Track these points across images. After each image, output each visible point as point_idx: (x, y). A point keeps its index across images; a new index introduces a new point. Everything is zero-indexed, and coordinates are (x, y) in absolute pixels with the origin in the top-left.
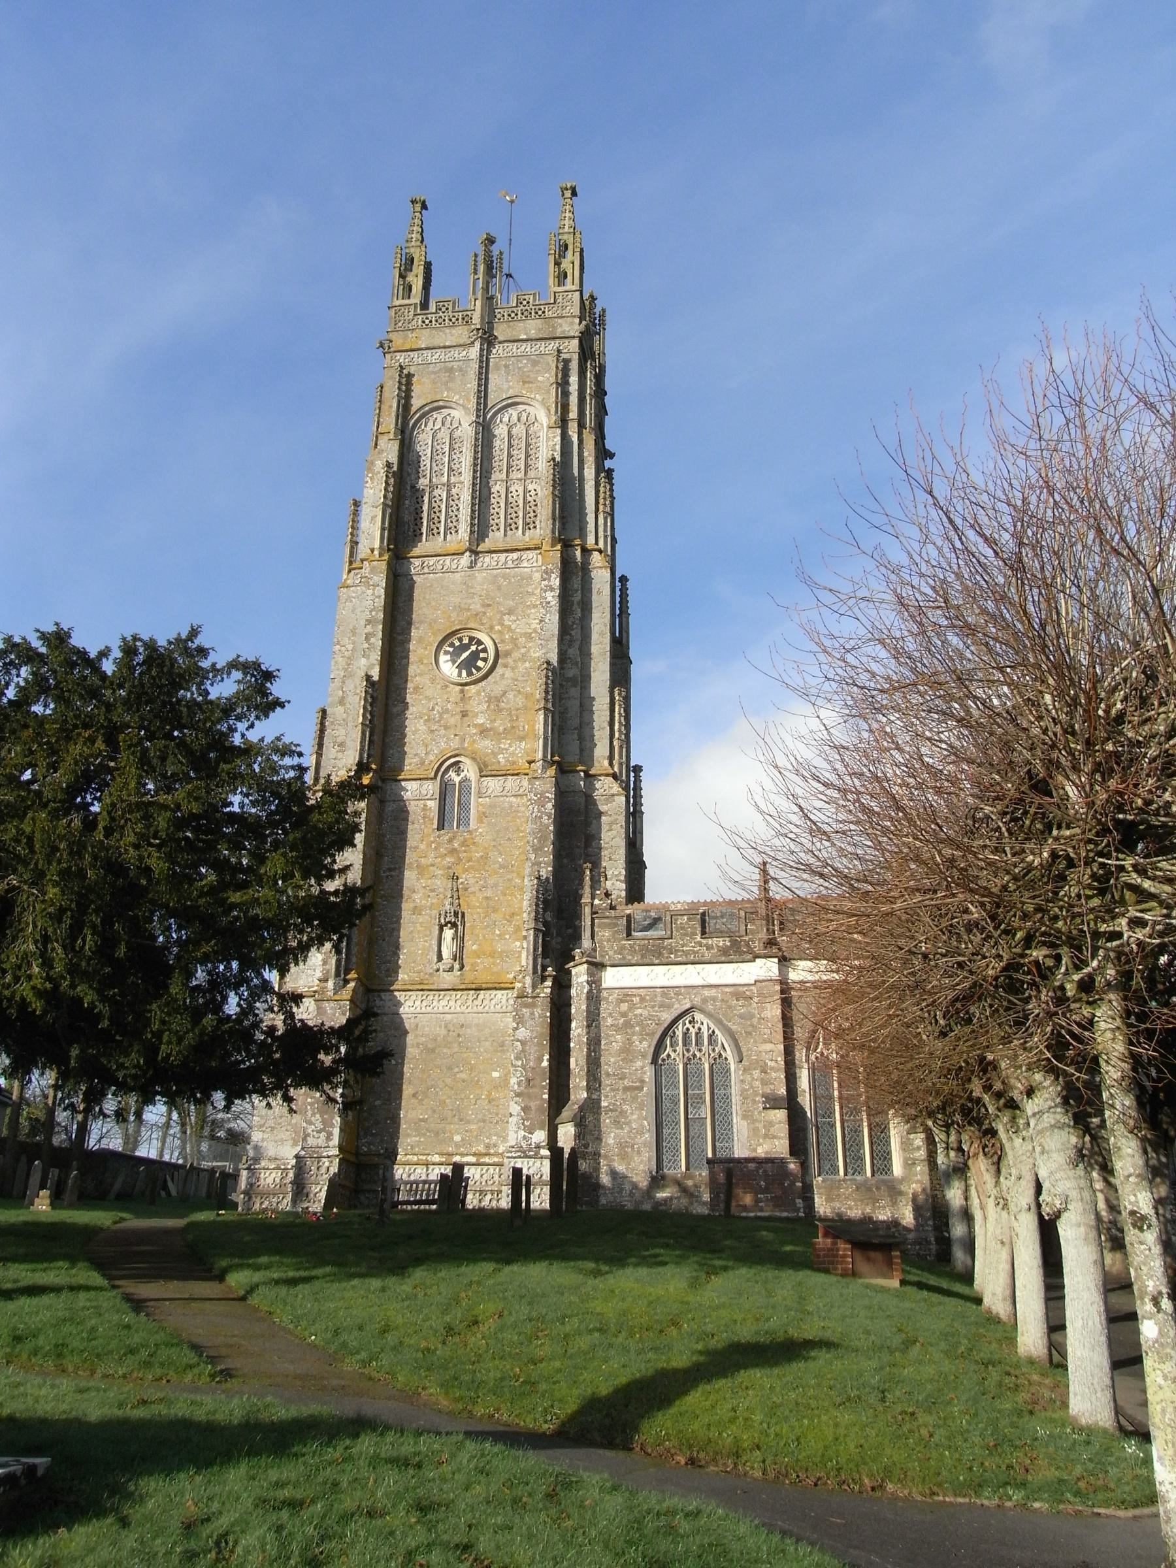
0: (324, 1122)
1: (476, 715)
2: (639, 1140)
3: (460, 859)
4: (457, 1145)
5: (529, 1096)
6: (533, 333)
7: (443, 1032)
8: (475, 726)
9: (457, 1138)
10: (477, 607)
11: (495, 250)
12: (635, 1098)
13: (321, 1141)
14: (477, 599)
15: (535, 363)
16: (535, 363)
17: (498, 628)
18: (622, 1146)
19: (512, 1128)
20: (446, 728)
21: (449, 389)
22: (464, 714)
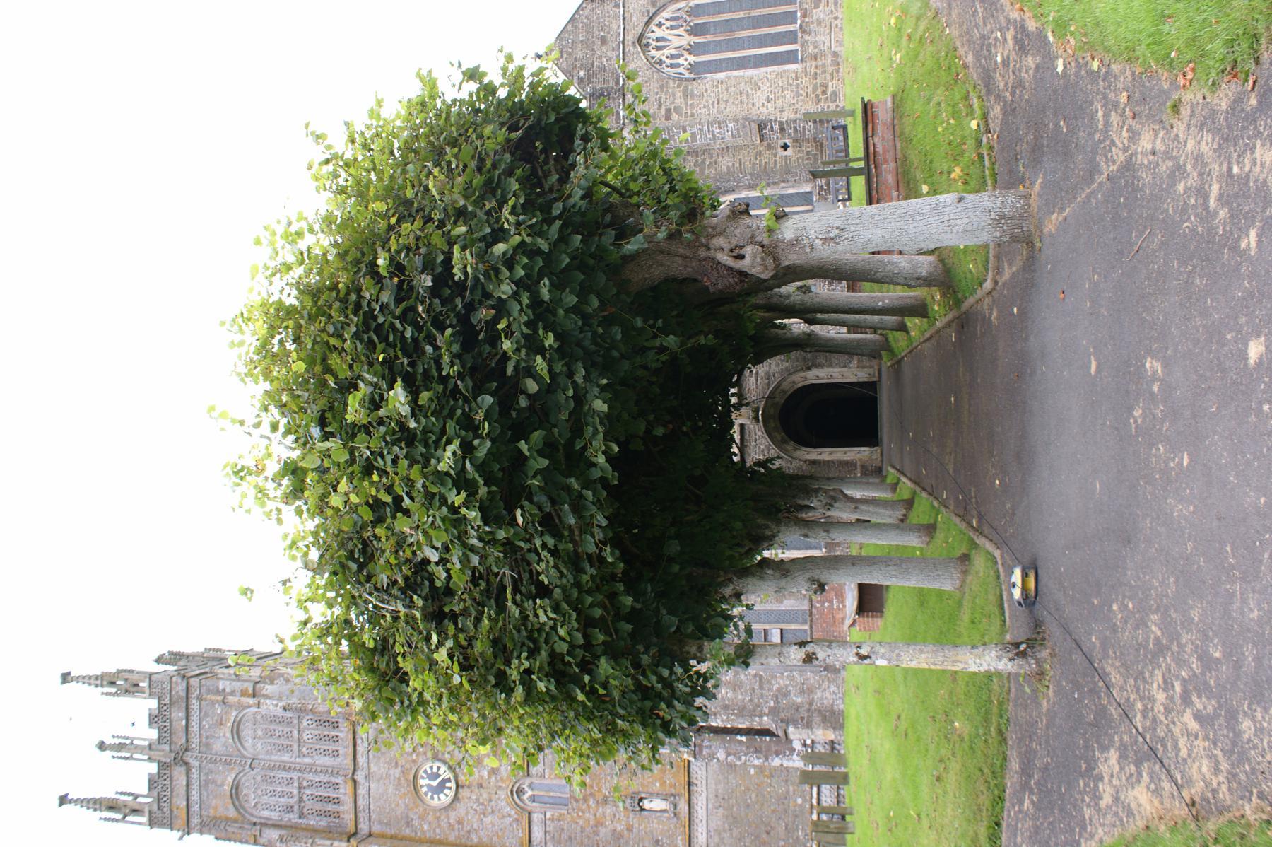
1: (482, 777)
2: (798, 679)
3: (591, 794)
4: (805, 801)
5: (768, 750)
6: (182, 714)
7: (721, 810)
8: (489, 777)
9: (799, 801)
10: (397, 772)
12: (769, 682)
14: (391, 772)
15: (206, 715)
17: (414, 757)
18: (802, 692)
19: (791, 764)
20: (490, 800)
21: (222, 785)
22: (480, 786)
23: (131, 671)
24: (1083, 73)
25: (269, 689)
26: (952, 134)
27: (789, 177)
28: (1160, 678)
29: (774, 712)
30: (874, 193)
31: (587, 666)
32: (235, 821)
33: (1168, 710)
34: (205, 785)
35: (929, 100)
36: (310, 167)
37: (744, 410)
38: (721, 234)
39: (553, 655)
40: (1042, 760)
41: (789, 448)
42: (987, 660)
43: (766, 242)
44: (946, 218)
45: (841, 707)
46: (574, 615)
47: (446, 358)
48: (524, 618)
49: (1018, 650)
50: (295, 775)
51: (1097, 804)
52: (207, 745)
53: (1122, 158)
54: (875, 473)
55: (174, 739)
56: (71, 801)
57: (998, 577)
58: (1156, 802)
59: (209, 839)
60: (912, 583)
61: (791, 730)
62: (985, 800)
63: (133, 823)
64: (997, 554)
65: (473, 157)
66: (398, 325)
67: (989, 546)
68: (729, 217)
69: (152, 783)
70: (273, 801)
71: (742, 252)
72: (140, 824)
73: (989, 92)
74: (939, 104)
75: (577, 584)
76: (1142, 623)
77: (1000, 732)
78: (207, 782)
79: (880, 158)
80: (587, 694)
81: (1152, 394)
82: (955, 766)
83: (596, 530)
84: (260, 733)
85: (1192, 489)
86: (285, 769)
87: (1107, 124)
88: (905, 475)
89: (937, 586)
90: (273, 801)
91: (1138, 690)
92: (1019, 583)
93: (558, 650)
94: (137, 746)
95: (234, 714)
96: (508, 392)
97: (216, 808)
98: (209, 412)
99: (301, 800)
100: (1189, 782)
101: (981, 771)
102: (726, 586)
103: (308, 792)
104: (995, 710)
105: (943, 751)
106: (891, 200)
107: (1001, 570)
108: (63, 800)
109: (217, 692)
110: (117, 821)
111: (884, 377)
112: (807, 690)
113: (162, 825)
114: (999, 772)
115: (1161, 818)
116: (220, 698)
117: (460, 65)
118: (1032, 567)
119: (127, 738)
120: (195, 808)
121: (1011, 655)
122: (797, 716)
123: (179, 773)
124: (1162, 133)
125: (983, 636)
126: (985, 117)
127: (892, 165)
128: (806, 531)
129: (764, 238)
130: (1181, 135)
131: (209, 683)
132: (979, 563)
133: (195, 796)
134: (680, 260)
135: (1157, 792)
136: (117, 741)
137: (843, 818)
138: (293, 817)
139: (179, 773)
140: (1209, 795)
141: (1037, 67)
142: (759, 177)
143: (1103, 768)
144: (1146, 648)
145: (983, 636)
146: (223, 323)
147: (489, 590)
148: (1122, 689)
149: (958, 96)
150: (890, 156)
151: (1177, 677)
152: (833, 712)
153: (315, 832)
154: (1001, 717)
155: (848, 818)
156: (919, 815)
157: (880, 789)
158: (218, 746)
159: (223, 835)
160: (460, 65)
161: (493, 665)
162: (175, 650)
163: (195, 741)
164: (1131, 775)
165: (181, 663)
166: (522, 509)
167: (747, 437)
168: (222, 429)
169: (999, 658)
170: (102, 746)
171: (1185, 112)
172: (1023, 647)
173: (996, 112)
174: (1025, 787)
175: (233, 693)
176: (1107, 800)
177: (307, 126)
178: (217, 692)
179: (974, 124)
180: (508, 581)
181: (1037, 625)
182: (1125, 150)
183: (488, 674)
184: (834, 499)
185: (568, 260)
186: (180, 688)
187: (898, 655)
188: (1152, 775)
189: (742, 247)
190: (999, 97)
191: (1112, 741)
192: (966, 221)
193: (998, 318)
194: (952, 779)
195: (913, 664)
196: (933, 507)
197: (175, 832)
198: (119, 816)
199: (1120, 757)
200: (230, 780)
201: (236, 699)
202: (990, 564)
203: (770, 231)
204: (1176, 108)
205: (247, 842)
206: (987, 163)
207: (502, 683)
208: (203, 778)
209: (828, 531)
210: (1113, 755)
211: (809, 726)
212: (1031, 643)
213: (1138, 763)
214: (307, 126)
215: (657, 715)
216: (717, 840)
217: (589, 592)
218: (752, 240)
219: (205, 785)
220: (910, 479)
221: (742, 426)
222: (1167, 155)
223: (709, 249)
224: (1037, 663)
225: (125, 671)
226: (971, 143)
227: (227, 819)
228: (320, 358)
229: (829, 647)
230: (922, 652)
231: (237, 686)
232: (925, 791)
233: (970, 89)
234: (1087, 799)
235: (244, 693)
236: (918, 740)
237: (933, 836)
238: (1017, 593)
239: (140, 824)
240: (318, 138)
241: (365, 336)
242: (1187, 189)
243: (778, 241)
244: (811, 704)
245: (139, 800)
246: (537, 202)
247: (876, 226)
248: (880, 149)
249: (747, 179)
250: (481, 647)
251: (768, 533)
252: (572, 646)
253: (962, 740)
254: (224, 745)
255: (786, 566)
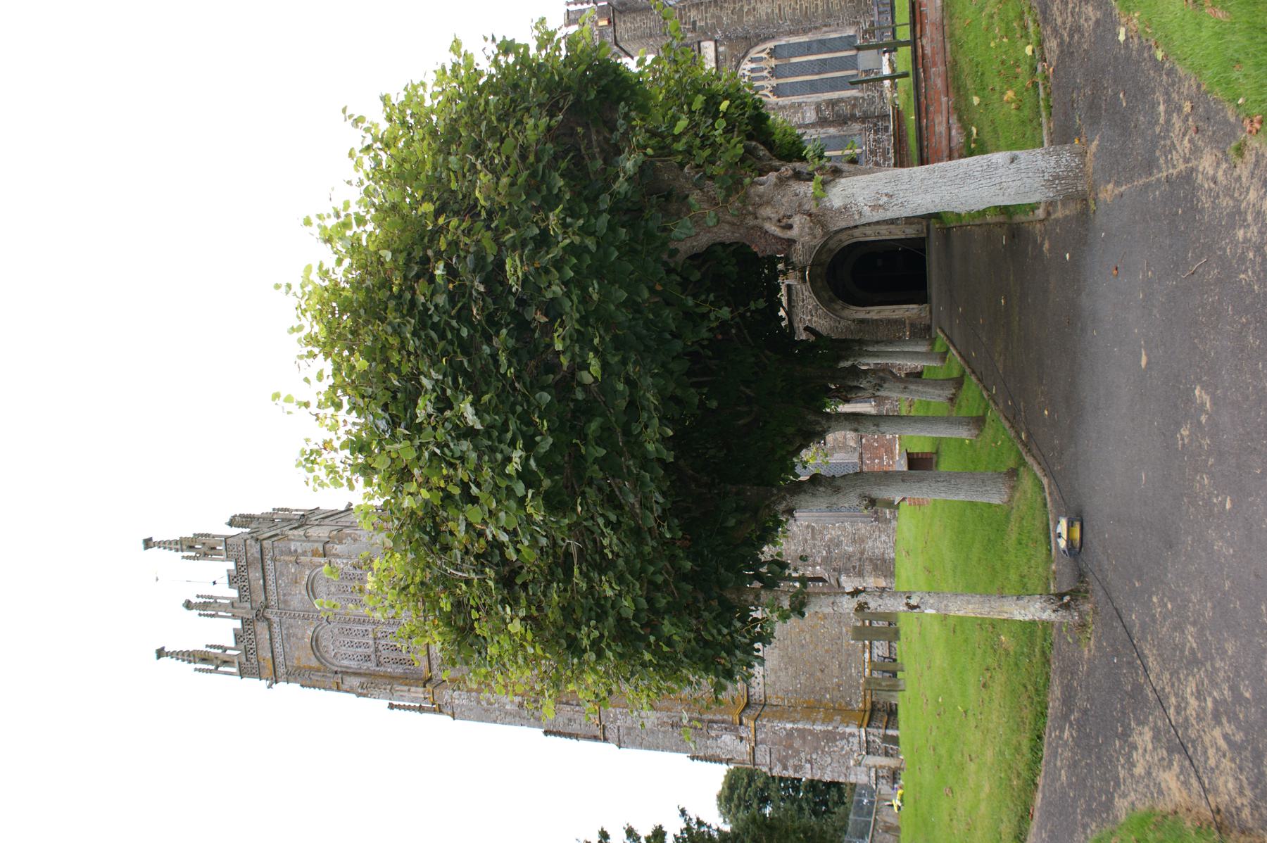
0: (841, 739)
6: (259, 574)
11: (194, 600)
13: (856, 740)
15: (282, 574)
16: (282, 574)
18: (854, 541)
21: (303, 638)
23: (207, 535)
24: (1146, 55)
25: (338, 548)
26: (1006, 53)
27: (832, 21)
28: (1194, 685)
29: (826, 561)
30: (922, 99)
31: (653, 627)
32: (318, 670)
33: (1199, 719)
34: (287, 638)
35: (982, 10)
36: (351, 155)
37: (791, 273)
38: (768, 203)
39: (620, 620)
40: (1081, 702)
41: (838, 307)
42: (1035, 610)
43: (814, 210)
44: (998, 180)
45: (892, 555)
46: (638, 585)
47: (503, 358)
48: (591, 588)
49: (1066, 599)
50: (370, 628)
51: (1130, 769)
52: (285, 602)
53: (1182, 166)
54: (922, 332)
55: (254, 597)
56: (167, 654)
57: (1045, 505)
58: (1185, 793)
59: (295, 687)
60: (961, 497)
61: (843, 578)
62: (1028, 714)
63: (226, 673)
64: (1045, 481)
65: (515, 147)
66: (454, 323)
67: (1036, 467)
68: (776, 185)
69: (238, 637)
70: (350, 651)
71: (790, 221)
72: (231, 674)
73: (1045, 20)
74: (992, 17)
75: (640, 555)
76: (1178, 627)
77: (1043, 653)
78: (288, 636)
79: (929, 62)
80: (654, 654)
81: (1199, 422)
82: (1000, 677)
83: (655, 506)
84: (333, 589)
85: (1232, 534)
86: (359, 622)
87: (1168, 121)
88: (954, 346)
89: (985, 500)
90: (350, 651)
91: (1173, 685)
92: (1064, 535)
93: (624, 615)
94: (220, 604)
95: (307, 572)
96: (565, 385)
97: (299, 659)
98: (274, 399)
99: (377, 650)
100: (1216, 791)
101: (1025, 687)
102: (780, 503)
103: (383, 642)
104: (1039, 633)
105: (989, 661)
106: (939, 161)
107: (1048, 499)
108: (160, 653)
109: (290, 553)
110: (211, 671)
111: (933, 235)
112: (858, 540)
113: (252, 675)
114: (1041, 690)
115: (1188, 810)
116: (293, 559)
117: (494, 40)
118: (1077, 517)
119: (211, 597)
120: (280, 659)
121: (1054, 607)
122: (849, 565)
123: (261, 627)
124: (1224, 166)
125: (1029, 560)
126: (1040, 44)
127: (941, 68)
128: (856, 426)
129: (810, 206)
130: (1244, 180)
131: (282, 544)
132: (1026, 483)
133: (279, 649)
134: (727, 227)
135: (1186, 784)
136: (202, 600)
137: (895, 675)
138: (371, 666)
139: (261, 627)
140: (1233, 810)
141: (1097, 22)
142: (799, 22)
143: (1135, 738)
144: (1182, 652)
145: (1029, 560)
146: (277, 287)
147: (560, 565)
148: (1158, 677)
149: (1012, 15)
150: (939, 59)
151: (1210, 694)
152: (884, 561)
153: (393, 678)
154: (1045, 640)
155: (900, 675)
156: (965, 712)
157: (929, 668)
158: (295, 603)
159: (308, 682)
160: (494, 40)
161: (563, 628)
162: (246, 513)
163: (273, 599)
164: (1163, 759)
165: (253, 526)
166: (584, 498)
167: (794, 297)
168: (289, 413)
169: (1044, 610)
170: (188, 605)
171: (1250, 157)
172: (1066, 599)
173: (1052, 44)
174: (1065, 717)
175: (304, 553)
176: (1139, 770)
177: (344, 111)
178: (290, 553)
179: (1029, 50)
180: (573, 550)
181: (1081, 576)
182: (1187, 161)
183: (563, 639)
184: (884, 380)
185: (616, 254)
186: (254, 550)
187: (946, 606)
188: (1182, 767)
189: (790, 217)
190: (1055, 31)
191: (1146, 718)
192: (1019, 183)
193: (1050, 250)
194: (997, 689)
195: (961, 613)
196: (982, 395)
197: (264, 681)
198: (212, 667)
199: (1154, 737)
200: (310, 633)
201: (308, 559)
202: (1037, 489)
203: (817, 199)
204: (1240, 151)
205: (330, 689)
206: (1042, 94)
207: (574, 647)
208: (284, 632)
209: (877, 425)
210: (1148, 735)
211: (860, 574)
212: (1074, 594)
213: (1170, 751)
214: (344, 111)
215: (719, 663)
216: (773, 678)
217: (651, 562)
218: (800, 210)
219: (287, 638)
220: (960, 353)
221: (789, 286)
222: (1228, 191)
223: (756, 218)
224: (1080, 615)
225: (202, 535)
226: (1024, 69)
227: (311, 669)
228: (378, 353)
229: (880, 597)
230: (969, 603)
231: (308, 546)
232: (972, 691)
233: (1026, 9)
234: (1122, 761)
235: (315, 553)
236: (966, 640)
237: (979, 735)
238: (1063, 543)
239: (231, 674)
240: (357, 121)
241: (423, 334)
242: (1246, 240)
243: (825, 208)
244: (862, 553)
245: (228, 652)
246: (586, 190)
247: (926, 191)
248: (928, 51)
249: (787, 25)
250: (553, 614)
251: (819, 428)
252: (638, 611)
253: (1008, 654)
254: (301, 601)
255: (838, 483)
